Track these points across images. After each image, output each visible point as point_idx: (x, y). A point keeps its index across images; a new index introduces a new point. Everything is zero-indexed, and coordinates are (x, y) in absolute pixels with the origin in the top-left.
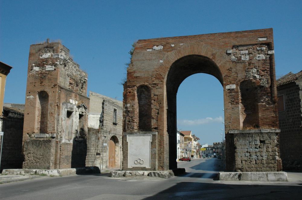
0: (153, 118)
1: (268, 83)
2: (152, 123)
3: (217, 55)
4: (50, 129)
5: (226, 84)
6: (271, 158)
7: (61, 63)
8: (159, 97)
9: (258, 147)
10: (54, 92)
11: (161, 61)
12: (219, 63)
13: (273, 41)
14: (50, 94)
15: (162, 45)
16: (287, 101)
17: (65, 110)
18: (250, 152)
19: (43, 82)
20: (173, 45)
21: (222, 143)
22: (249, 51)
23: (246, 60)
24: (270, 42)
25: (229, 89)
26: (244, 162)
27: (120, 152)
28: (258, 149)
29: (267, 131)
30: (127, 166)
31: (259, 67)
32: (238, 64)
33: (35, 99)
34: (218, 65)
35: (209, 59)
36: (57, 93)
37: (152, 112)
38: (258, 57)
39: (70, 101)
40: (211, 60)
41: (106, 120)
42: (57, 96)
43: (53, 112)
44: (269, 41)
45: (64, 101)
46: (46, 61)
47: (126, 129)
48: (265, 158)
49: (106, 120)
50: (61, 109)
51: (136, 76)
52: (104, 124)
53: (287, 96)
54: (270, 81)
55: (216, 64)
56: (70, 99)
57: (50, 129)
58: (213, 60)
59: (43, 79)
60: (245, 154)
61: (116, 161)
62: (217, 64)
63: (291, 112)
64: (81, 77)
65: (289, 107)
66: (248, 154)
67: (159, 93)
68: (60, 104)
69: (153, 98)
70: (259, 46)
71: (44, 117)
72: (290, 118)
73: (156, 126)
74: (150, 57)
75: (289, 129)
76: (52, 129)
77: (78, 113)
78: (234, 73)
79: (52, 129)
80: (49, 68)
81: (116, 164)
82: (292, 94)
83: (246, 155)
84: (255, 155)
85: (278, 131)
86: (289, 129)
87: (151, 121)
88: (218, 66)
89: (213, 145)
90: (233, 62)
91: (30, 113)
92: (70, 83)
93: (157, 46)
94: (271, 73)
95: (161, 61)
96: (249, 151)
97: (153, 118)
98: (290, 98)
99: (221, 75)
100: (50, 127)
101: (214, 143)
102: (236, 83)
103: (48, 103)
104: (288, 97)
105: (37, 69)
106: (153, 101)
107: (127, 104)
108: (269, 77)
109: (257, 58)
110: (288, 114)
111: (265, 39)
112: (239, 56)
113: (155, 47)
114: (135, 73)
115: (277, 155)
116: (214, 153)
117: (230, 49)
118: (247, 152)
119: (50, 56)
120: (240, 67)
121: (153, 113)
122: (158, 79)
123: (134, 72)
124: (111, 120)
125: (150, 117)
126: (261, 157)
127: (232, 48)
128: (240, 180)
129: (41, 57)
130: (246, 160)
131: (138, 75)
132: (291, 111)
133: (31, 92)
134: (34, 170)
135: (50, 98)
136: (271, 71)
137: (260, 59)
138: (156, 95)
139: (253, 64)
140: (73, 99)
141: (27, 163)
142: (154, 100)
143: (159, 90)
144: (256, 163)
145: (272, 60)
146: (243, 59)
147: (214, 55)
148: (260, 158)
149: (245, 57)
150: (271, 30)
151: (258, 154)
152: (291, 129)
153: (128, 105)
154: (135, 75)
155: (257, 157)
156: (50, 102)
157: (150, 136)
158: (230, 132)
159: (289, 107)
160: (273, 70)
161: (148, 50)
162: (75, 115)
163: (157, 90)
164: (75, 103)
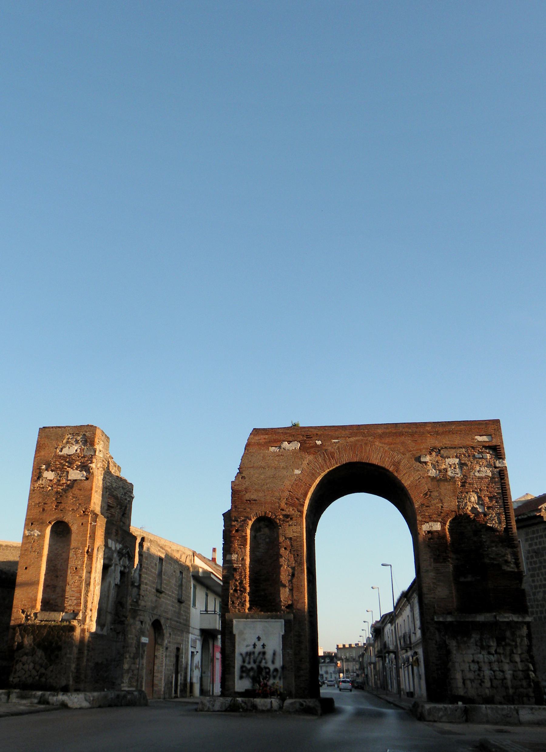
0: (285, 586)
1: (500, 523)
2: (281, 596)
3: (402, 464)
4: (70, 603)
5: (422, 521)
6: (520, 675)
7: (99, 466)
8: (295, 544)
9: (494, 652)
10: (82, 524)
11: (297, 472)
12: (406, 481)
13: (502, 443)
14: (74, 528)
15: (299, 442)
16: (529, 555)
17: (100, 562)
18: (478, 663)
19: (61, 503)
20: (319, 443)
21: (454, 640)
22: (460, 460)
23: (457, 475)
24: (497, 444)
25: (429, 532)
26: (468, 682)
27: (164, 659)
28: (493, 655)
29: (508, 618)
30: (234, 688)
31: (481, 490)
32: (442, 484)
33: (42, 537)
34: (406, 482)
35: (388, 470)
36: (89, 525)
37: (282, 573)
38: (479, 471)
39: (109, 541)
40: (392, 473)
41: (146, 584)
42: (89, 532)
43: (79, 567)
44: (494, 443)
45: (100, 543)
46: (69, 460)
47: (229, 606)
48: (509, 675)
49: (146, 584)
50: (94, 559)
51: (248, 498)
52: (142, 593)
53: (528, 543)
54: (503, 517)
55: (400, 481)
56: (109, 540)
57: (70, 603)
58: (396, 474)
59: (61, 496)
60: (469, 666)
61: (156, 682)
62: (403, 482)
63: (539, 578)
64: (125, 491)
65: (534, 566)
66: (474, 667)
67: (295, 534)
68: (93, 550)
69: (284, 545)
70: (478, 450)
71: (57, 577)
72: (540, 592)
73: (290, 602)
74: (276, 463)
75: (539, 615)
76: (76, 601)
77: (119, 569)
78: (435, 501)
79: (76, 601)
80: (75, 474)
81: (155, 689)
82: (537, 539)
83: (472, 668)
84: (489, 668)
85: (62, 613)
86: (539, 615)
87: (280, 591)
88: (405, 485)
89: (336, 651)
90: (433, 479)
91: (30, 566)
92: (108, 506)
93: (289, 442)
94: (504, 503)
95: (297, 472)
96: (476, 659)
97: (285, 586)
98: (535, 547)
99: (412, 504)
100: (72, 598)
101: (338, 646)
102: (440, 520)
103: (69, 545)
104: (531, 545)
105: (49, 475)
106: (282, 551)
107: (231, 554)
108: (502, 510)
109: (477, 474)
110: (533, 581)
111: (485, 438)
112: (443, 467)
113: (285, 444)
114: (246, 492)
115: (531, 671)
116: (340, 673)
117: (426, 455)
118: (473, 661)
119: (79, 450)
120: (446, 488)
121: (284, 577)
122: (293, 505)
123: (246, 490)
124: (154, 583)
125: (277, 583)
126: (502, 674)
127: (430, 452)
128: (467, 721)
129: (60, 453)
130: (473, 677)
131: (253, 497)
132: (538, 576)
133: (34, 523)
134: (39, 693)
135: (74, 536)
136: (504, 500)
137: (483, 475)
138: (288, 538)
139: (470, 484)
140: (112, 540)
141: (19, 677)
142: (285, 549)
143: (294, 527)
144: (492, 686)
145: (504, 478)
146: (449, 473)
147: (397, 464)
148: (499, 675)
149: (454, 471)
150: (497, 422)
151: (496, 667)
152: (543, 615)
153: (234, 557)
154: (248, 496)
155: (494, 671)
156: (73, 544)
157: (279, 624)
158: (437, 618)
159: (534, 566)
160: (507, 498)
161: (272, 449)
162: (114, 573)
163: (291, 528)
164: (116, 548)
